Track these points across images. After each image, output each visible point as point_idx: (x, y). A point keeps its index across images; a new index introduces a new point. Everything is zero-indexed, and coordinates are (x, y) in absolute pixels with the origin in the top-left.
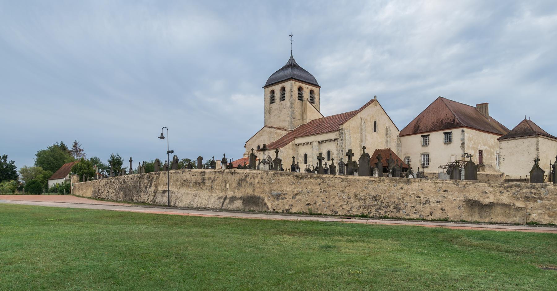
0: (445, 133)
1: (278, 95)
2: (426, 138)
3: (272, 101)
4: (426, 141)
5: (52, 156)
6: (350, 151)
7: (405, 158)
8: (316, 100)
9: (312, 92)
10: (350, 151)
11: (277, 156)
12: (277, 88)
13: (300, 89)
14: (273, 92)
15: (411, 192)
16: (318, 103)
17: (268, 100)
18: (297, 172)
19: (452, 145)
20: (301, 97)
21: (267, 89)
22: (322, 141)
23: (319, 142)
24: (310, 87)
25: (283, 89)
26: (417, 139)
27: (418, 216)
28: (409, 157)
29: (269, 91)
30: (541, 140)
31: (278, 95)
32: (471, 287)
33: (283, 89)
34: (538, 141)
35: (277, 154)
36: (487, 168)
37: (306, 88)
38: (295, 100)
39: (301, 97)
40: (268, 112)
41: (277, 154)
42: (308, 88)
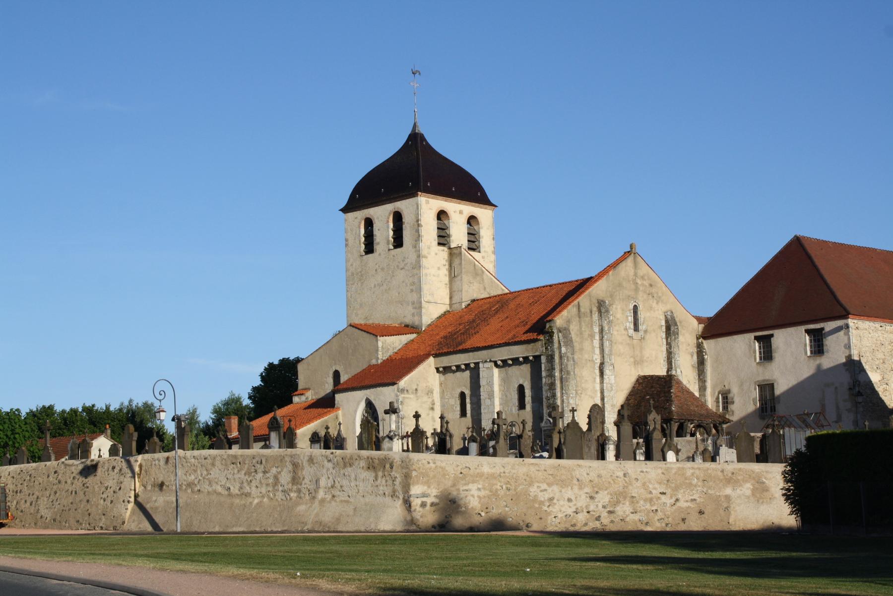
1: (384, 232)
2: (766, 342)
3: (370, 248)
5: (550, 321)
6: (416, 412)
10: (416, 412)
11: (417, 425)
12: (382, 214)
13: (442, 215)
14: (369, 223)
15: (651, 486)
18: (573, 498)
20: (443, 238)
21: (351, 215)
25: (398, 217)
26: (743, 346)
31: (384, 232)
33: (398, 217)
35: (417, 421)
36: (799, 447)
39: (443, 238)
40: (355, 278)
41: (417, 421)
42: (461, 212)
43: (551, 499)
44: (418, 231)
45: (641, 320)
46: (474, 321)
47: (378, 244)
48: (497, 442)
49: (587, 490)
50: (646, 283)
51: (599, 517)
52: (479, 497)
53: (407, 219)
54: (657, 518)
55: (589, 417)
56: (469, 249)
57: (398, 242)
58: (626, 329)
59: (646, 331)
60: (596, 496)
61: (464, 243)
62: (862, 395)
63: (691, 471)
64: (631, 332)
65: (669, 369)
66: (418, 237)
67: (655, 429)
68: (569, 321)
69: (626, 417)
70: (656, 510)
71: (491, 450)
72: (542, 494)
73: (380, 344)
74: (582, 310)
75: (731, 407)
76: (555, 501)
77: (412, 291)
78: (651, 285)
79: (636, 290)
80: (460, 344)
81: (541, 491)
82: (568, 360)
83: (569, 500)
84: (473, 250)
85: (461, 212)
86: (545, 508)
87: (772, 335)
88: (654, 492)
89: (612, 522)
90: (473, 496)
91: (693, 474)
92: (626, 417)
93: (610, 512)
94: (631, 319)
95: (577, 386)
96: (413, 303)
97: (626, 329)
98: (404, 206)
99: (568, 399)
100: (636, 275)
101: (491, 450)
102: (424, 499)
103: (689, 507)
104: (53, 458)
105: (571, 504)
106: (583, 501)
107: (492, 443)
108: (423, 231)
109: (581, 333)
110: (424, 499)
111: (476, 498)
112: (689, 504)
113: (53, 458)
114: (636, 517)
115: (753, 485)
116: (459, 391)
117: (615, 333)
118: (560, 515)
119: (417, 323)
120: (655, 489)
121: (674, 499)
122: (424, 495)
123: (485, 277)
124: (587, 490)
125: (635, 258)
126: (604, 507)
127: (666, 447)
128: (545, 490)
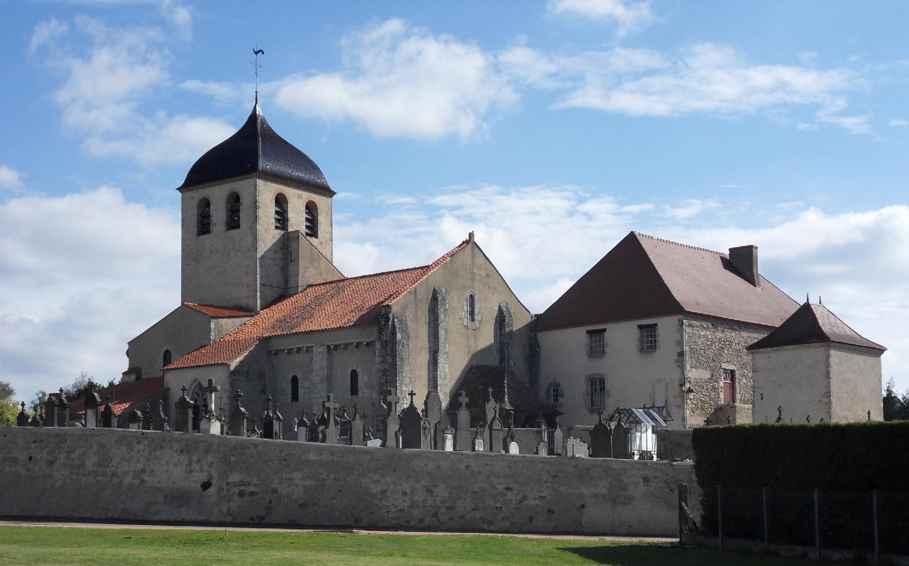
0: (640, 327)
1: (219, 214)
4: (597, 346)
7: (550, 385)
8: (322, 228)
9: (311, 209)
12: (218, 194)
13: (281, 201)
14: (205, 204)
15: (495, 480)
16: (327, 236)
17: (194, 229)
18: (408, 491)
19: (657, 355)
22: (337, 347)
23: (329, 347)
24: (307, 196)
27: (508, 524)
28: (558, 385)
29: (195, 202)
30: (835, 356)
31: (219, 214)
32: (371, 562)
33: (234, 201)
34: (828, 356)
37: (297, 200)
38: (267, 230)
39: (282, 220)
43: (384, 492)
44: (255, 213)
45: (476, 310)
46: (309, 305)
47: (215, 225)
48: (327, 427)
49: (423, 482)
50: (483, 273)
51: (437, 513)
52: (303, 486)
53: (245, 201)
54: (500, 516)
55: (426, 403)
56: (307, 234)
57: (233, 223)
58: (461, 319)
59: (480, 322)
60: (434, 490)
61: (303, 229)
62: (692, 391)
63: (541, 465)
64: (466, 322)
65: (502, 360)
66: (255, 220)
67: (494, 418)
68: (405, 307)
69: (464, 405)
70: (501, 508)
71: (321, 436)
72: (373, 485)
73: (213, 326)
74: (419, 297)
75: (560, 400)
76: (388, 494)
77: (247, 273)
78: (488, 276)
79: (473, 280)
80: (295, 326)
81: (373, 482)
82: (403, 346)
83: (404, 493)
84: (311, 235)
85: (300, 197)
86: (376, 502)
87: (605, 330)
88: (499, 487)
89: (451, 519)
90: (297, 486)
91: (543, 469)
92: (464, 405)
93: (448, 508)
94: (467, 308)
95: (410, 373)
96: (248, 286)
97: (461, 319)
98: (240, 186)
99: (401, 386)
100: (473, 263)
101: (321, 436)
102: (243, 488)
103: (537, 506)
104: (56, 422)
105: (406, 498)
106: (420, 496)
107: (321, 428)
108: (260, 213)
109: (417, 320)
110: (243, 488)
111: (300, 488)
112: (538, 502)
113: (56, 422)
114: (478, 515)
115: (610, 483)
116: (291, 375)
117: (451, 322)
118: (393, 510)
119: (251, 306)
120: (500, 484)
121: (520, 496)
122: (242, 483)
123: (322, 263)
124: (423, 482)
125: (473, 251)
126: (443, 502)
127: (509, 439)
128: (378, 481)
